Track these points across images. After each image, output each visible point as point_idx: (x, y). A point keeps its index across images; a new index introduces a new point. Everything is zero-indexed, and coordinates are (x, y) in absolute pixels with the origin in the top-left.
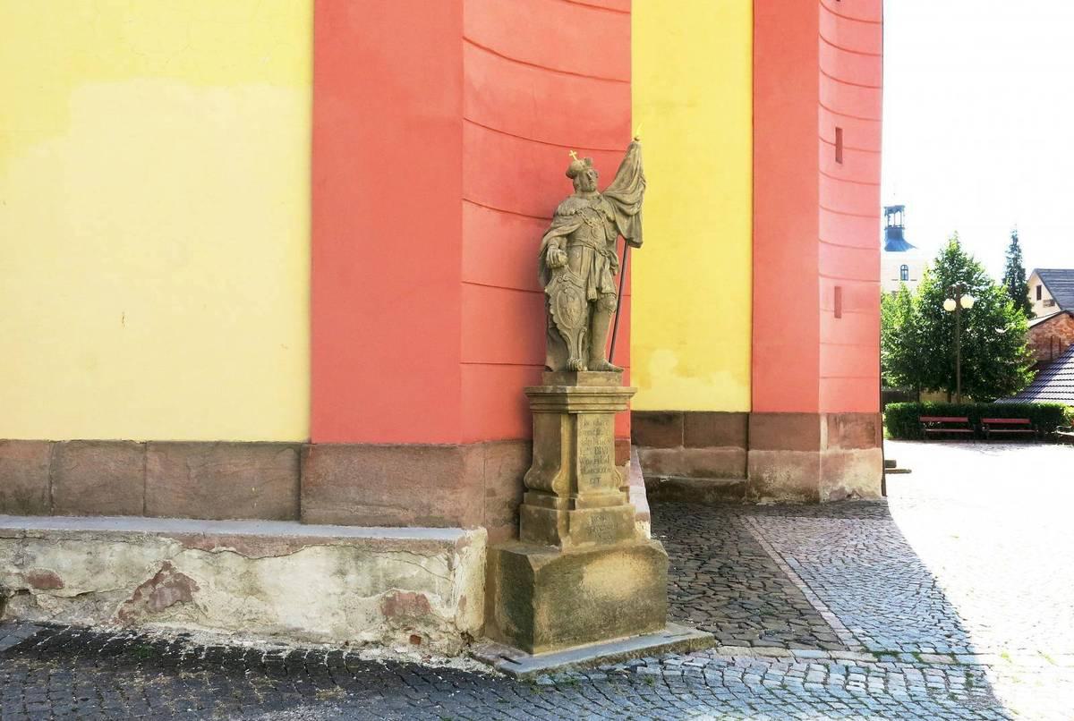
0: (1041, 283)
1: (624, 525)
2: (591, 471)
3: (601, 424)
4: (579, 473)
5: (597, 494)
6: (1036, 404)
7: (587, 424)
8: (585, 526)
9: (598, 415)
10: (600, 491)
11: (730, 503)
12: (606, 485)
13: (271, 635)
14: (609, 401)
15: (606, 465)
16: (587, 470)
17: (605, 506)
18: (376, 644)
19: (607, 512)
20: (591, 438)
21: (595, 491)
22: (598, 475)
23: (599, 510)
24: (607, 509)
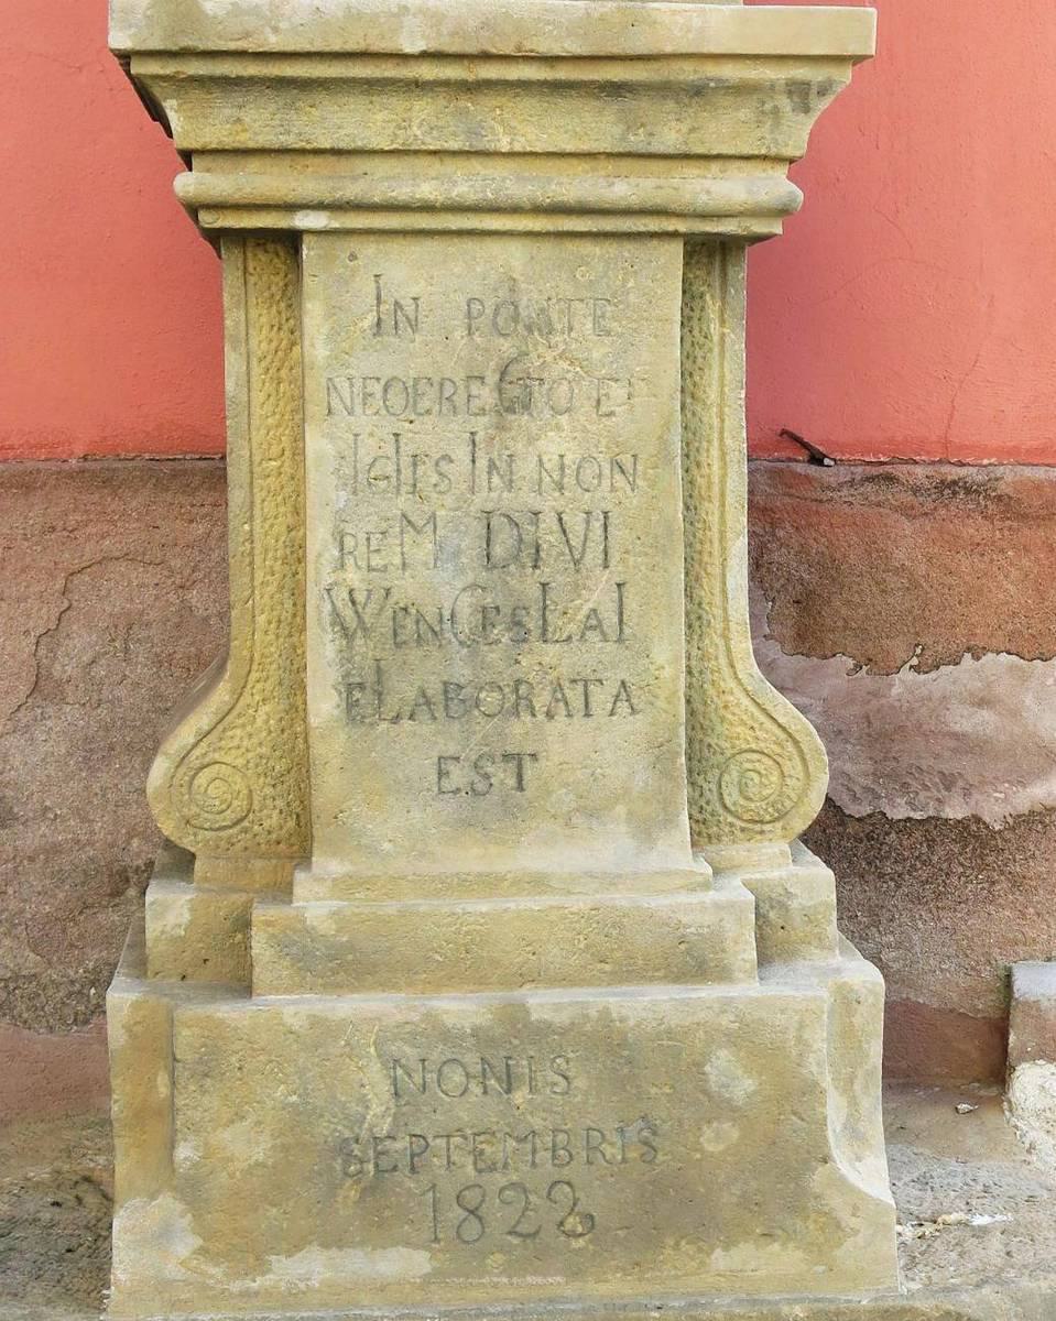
0: (907, 666)
1: (717, 1140)
2: (451, 701)
3: (542, 326)
4: (324, 705)
5: (490, 884)
6: (222, 1022)
7: (393, 320)
8: (327, 1129)
9: (515, 255)
10: (530, 858)
11: (726, 1076)
12: (591, 810)
13: (697, 721)
14: (597, 126)
15: (594, 653)
16: (403, 689)
17: (525, 978)
18: (352, 385)
19: (542, 1031)
20: (442, 435)
21: (471, 858)
22: (518, 731)
23: (461, 1009)
24: (543, 1003)
